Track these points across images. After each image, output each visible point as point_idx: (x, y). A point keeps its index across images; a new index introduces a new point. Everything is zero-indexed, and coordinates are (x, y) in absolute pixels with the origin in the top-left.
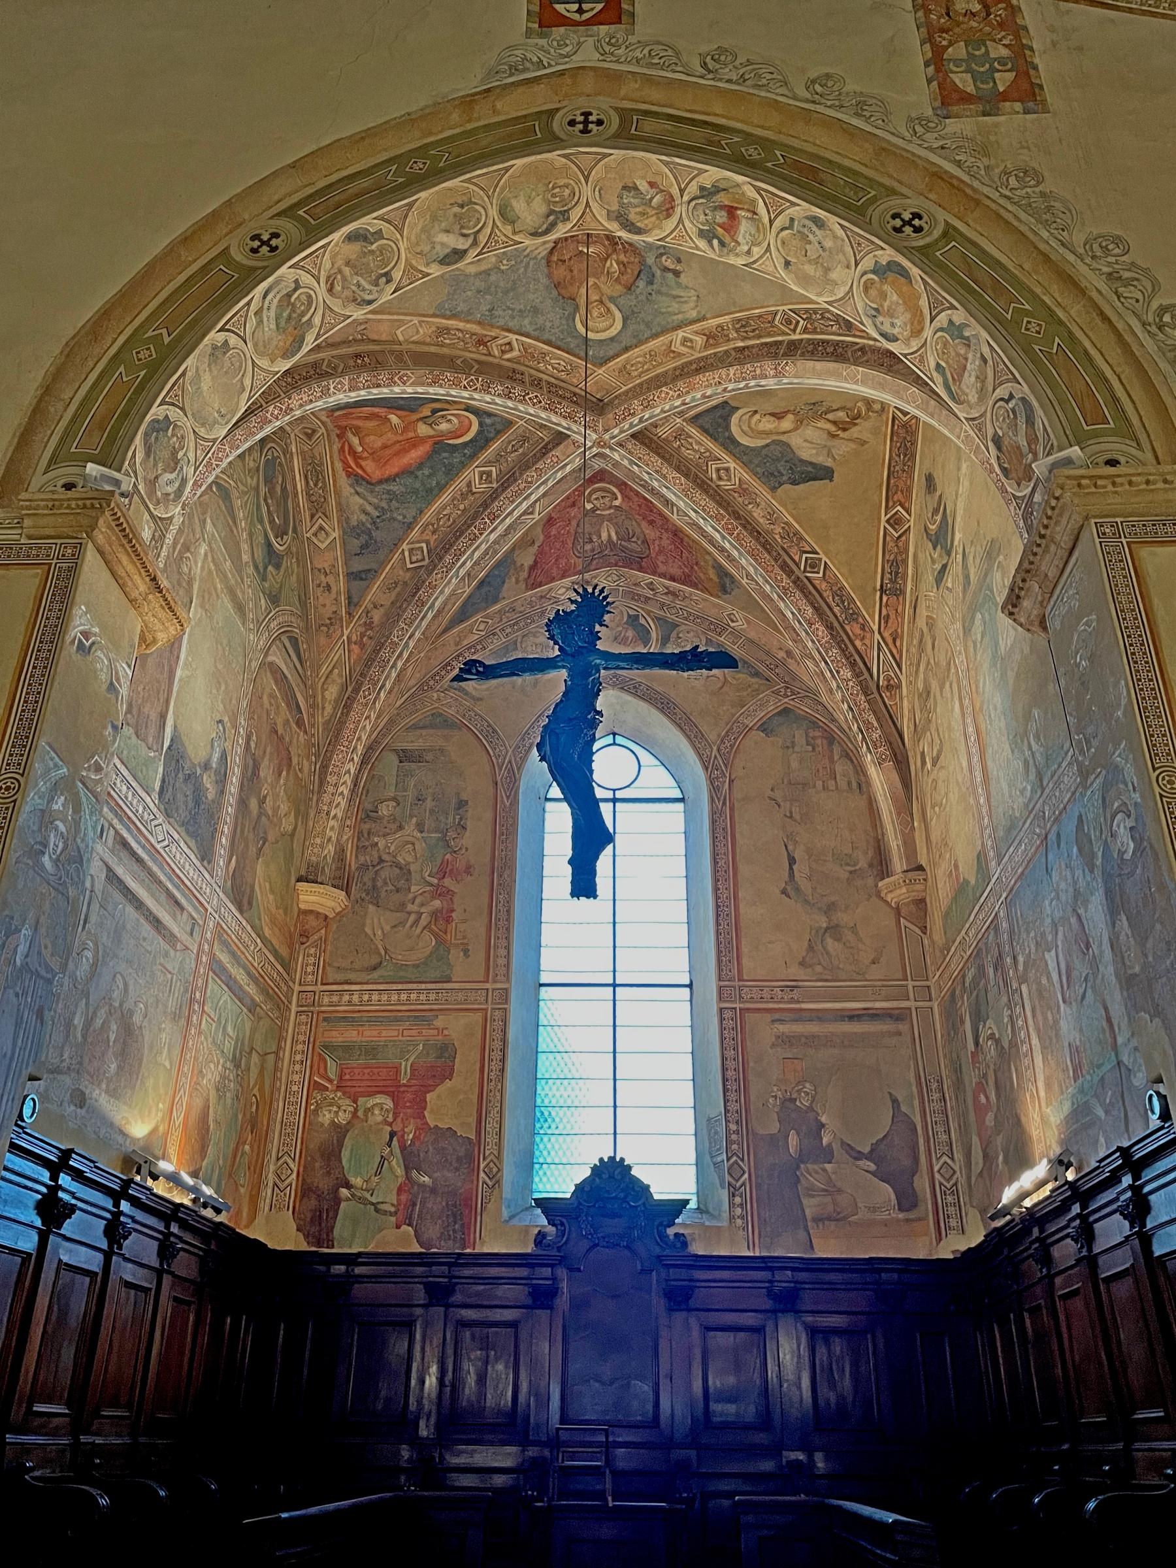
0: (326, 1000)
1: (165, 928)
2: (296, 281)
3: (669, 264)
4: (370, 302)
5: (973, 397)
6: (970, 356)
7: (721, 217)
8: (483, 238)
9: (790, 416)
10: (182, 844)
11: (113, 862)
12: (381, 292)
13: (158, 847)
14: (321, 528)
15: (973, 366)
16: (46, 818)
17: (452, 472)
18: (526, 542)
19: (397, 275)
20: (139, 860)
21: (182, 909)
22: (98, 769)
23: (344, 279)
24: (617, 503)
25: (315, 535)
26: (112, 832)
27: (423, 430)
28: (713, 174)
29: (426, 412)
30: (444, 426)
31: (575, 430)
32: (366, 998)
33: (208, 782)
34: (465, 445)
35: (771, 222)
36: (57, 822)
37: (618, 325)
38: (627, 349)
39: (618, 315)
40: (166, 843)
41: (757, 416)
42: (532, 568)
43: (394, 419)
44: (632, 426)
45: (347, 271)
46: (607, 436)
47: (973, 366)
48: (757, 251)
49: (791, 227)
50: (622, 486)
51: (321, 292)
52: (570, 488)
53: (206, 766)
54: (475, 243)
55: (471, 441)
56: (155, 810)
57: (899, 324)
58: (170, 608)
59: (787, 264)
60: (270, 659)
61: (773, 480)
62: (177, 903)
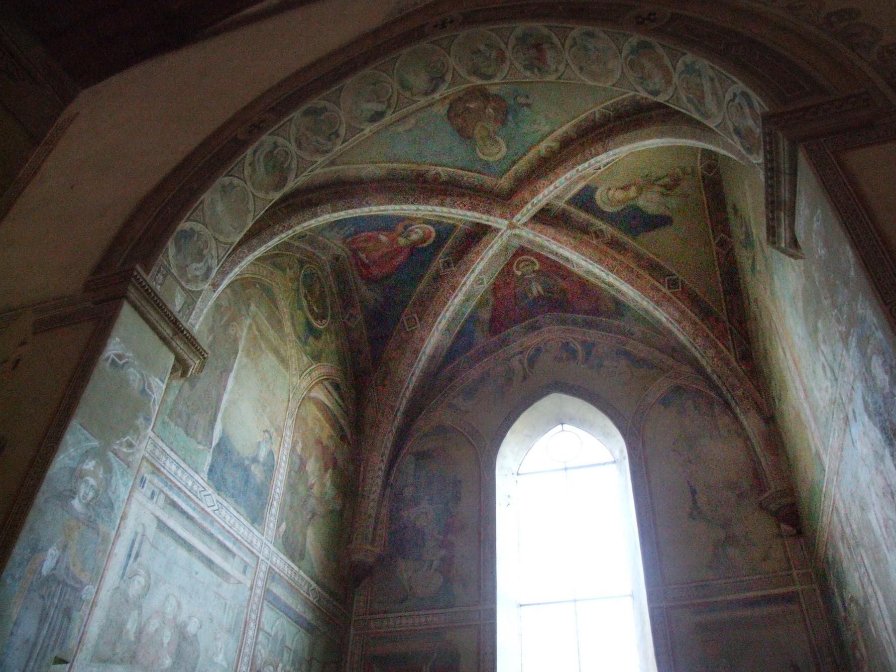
0: (372, 625)
1: (218, 567)
2: (275, 143)
3: (522, 100)
4: (327, 152)
5: (714, 110)
6: (704, 82)
7: (533, 53)
8: (393, 102)
9: (633, 188)
10: (232, 509)
11: (164, 517)
12: (334, 144)
13: (209, 510)
14: (351, 315)
15: (707, 87)
16: (77, 475)
17: (425, 265)
18: (482, 304)
19: (342, 132)
20: (190, 518)
21: (234, 555)
22: (130, 445)
23: (308, 138)
24: (537, 268)
25: (348, 320)
26: (162, 496)
27: (402, 241)
28: (520, 27)
29: (400, 228)
30: (414, 237)
31: (499, 223)
32: (398, 622)
33: (257, 471)
34: (429, 246)
35: (563, 45)
36: (88, 478)
37: (504, 149)
38: (514, 163)
39: (501, 142)
40: (216, 508)
41: (611, 192)
42: (492, 320)
43: (383, 238)
44: (528, 211)
45: (308, 134)
46: (514, 221)
47: (707, 87)
48: (561, 67)
49: (575, 43)
50: (539, 256)
51: (293, 147)
52: (502, 262)
53: (255, 460)
54: (389, 106)
55: (434, 241)
56: (205, 485)
57: (657, 81)
58: (192, 343)
59: (581, 69)
60: (313, 394)
61: (633, 231)
62: (228, 549)
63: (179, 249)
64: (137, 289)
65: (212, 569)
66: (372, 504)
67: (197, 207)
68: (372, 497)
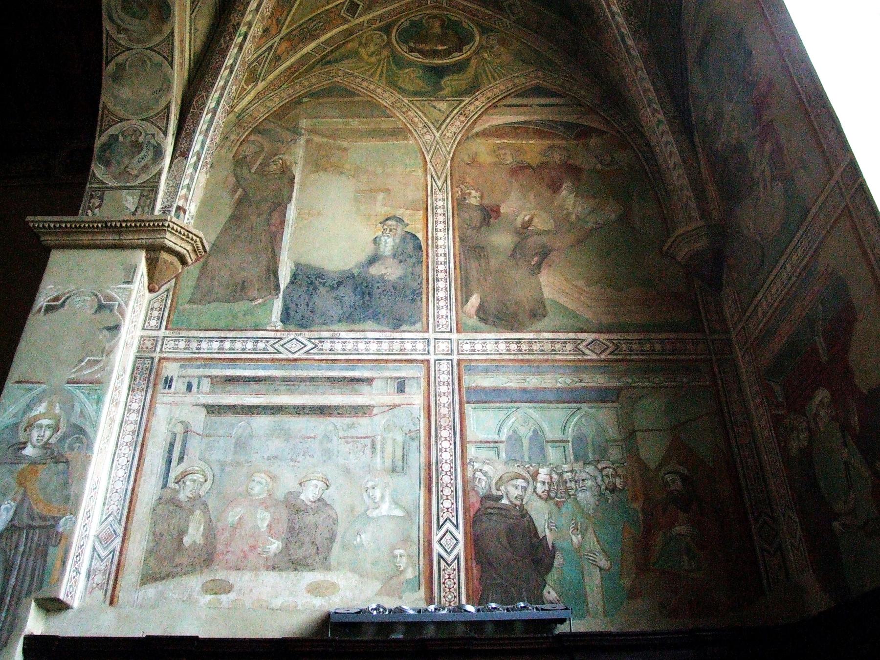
20: (257, 380)
21: (369, 381)
63: (107, 164)
64: (50, 233)
65: (330, 415)
66: (675, 174)
67: (102, 115)
68: (671, 164)
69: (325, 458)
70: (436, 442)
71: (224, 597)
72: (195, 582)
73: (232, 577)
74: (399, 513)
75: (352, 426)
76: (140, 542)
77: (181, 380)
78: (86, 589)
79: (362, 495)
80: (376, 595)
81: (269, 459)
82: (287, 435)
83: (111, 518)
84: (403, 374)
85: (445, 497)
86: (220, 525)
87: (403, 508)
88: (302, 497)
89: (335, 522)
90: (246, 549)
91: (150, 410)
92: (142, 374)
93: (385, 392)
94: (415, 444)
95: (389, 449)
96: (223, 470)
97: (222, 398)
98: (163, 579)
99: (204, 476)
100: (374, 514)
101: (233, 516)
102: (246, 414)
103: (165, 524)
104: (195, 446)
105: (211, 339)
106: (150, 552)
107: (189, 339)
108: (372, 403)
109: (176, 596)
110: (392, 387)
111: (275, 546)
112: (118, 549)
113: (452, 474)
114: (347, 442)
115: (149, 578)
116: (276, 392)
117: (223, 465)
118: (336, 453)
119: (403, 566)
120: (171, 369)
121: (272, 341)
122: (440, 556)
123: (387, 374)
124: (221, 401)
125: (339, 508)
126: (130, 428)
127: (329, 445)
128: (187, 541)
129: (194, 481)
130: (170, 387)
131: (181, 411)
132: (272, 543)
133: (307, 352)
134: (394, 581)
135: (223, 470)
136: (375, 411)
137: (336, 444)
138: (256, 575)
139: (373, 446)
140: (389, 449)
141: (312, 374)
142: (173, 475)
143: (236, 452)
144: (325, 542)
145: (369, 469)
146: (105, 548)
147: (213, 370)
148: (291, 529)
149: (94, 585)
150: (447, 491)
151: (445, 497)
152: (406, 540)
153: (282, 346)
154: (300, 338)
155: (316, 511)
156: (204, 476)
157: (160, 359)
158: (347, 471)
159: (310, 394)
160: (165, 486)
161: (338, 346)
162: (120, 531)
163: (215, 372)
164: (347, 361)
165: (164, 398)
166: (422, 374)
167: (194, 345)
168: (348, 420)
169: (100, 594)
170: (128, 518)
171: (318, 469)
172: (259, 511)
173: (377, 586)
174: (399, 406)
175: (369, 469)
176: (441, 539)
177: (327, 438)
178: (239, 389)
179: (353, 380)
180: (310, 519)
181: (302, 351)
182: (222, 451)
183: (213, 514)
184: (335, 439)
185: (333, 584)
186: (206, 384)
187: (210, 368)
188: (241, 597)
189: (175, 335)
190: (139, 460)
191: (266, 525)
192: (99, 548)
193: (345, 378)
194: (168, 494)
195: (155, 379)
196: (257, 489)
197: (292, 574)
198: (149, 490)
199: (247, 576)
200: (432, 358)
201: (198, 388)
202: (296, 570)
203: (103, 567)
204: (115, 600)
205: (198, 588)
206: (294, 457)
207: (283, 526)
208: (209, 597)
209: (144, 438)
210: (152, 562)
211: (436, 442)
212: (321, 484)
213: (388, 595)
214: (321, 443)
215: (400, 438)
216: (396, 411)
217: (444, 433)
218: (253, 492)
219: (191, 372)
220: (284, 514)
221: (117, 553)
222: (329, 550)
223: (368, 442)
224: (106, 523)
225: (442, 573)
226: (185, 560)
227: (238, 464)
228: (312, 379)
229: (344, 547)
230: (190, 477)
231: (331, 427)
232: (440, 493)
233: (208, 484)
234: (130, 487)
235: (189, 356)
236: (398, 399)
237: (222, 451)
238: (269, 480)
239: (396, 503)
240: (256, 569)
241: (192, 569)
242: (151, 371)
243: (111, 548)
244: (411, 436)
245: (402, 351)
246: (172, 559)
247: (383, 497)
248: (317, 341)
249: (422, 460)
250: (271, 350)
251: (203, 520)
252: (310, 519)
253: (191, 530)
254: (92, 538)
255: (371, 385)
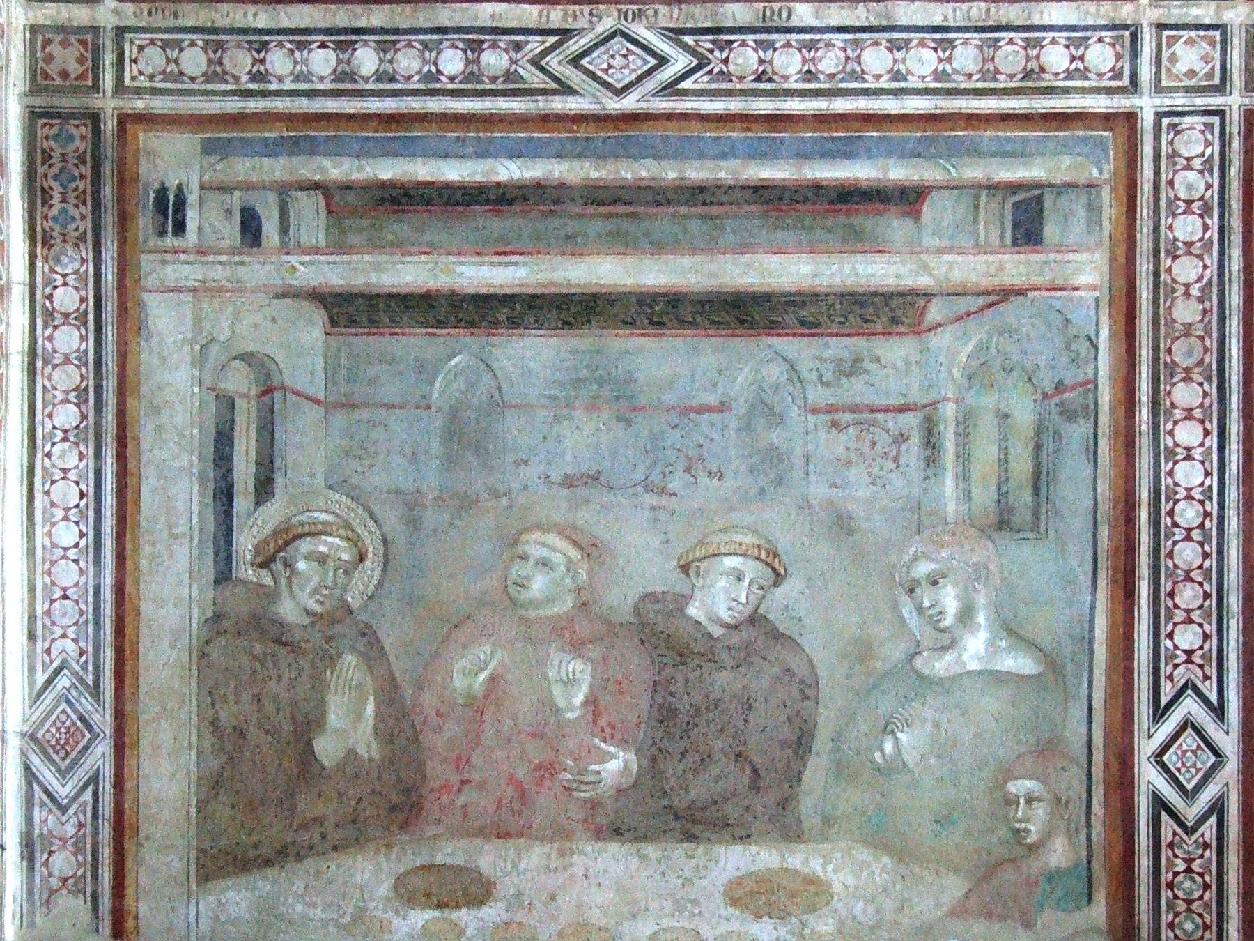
21: (909, 199)
65: (773, 327)
69: (762, 482)
70: (1155, 427)
71: (464, 916)
72: (370, 874)
73: (488, 858)
74: (1020, 663)
75: (853, 368)
76: (174, 754)
77: (214, 199)
78: (30, 892)
79: (896, 608)
80: (952, 913)
81: (568, 482)
82: (624, 401)
83: (63, 682)
84: (1036, 172)
85: (1179, 616)
86: (429, 700)
87: (1033, 646)
88: (693, 611)
89: (808, 688)
90: (521, 774)
91: (123, 308)
92: (64, 177)
93: (968, 243)
94: (1078, 431)
95: (986, 452)
96: (413, 523)
97: (377, 268)
98: (268, 863)
99: (355, 541)
100: (942, 666)
101: (468, 670)
102: (471, 324)
103: (246, 697)
104: (307, 445)
105: (300, 37)
106: (213, 786)
107: (215, 40)
108: (924, 281)
109: (318, 913)
110: (993, 223)
111: (616, 765)
112: (108, 770)
113: (1207, 538)
114: (835, 424)
115: (219, 862)
116: (572, 246)
117: (412, 505)
118: (798, 462)
119: (1034, 832)
120: (170, 160)
121: (535, 45)
122: (1159, 804)
123: (974, 172)
124: (373, 278)
125: (820, 648)
126: (66, 378)
127: (775, 437)
128: (327, 749)
129: (322, 560)
130: (180, 228)
131: (236, 317)
132: (605, 758)
133: (671, 89)
134: (1008, 876)
135: (413, 523)
136: (935, 312)
137: (800, 434)
138: (562, 853)
139: (931, 441)
140: (986, 452)
141: (697, 172)
142: (245, 543)
143: (451, 462)
144: (781, 755)
145: (920, 519)
146: (63, 774)
147: (326, 162)
148: (665, 715)
149: (54, 882)
150: (1188, 596)
151: (1179, 616)
152: (1047, 750)
153: (575, 61)
154: (641, 31)
155: (744, 658)
156: (355, 541)
157: (124, 120)
158: (842, 524)
159: (694, 251)
160: (224, 576)
161: (789, 63)
162: (103, 719)
163: (336, 169)
164: (822, 120)
165: (167, 271)
166: (1108, 168)
167: (240, 62)
168: (837, 347)
169: (78, 907)
170: (119, 675)
171: (736, 517)
172: (555, 656)
173: (955, 888)
174: (1020, 292)
175: (920, 519)
176: (1166, 747)
177: (765, 410)
178: (434, 234)
179: (850, 196)
180: (723, 681)
181: (650, 85)
182: (401, 456)
183: (400, 666)
184: (794, 413)
185: (812, 881)
186: (310, 217)
187: (313, 153)
188: (519, 917)
189: (158, 21)
190: (121, 492)
191: (579, 699)
192: (47, 775)
193: (817, 187)
194: (238, 604)
195: (121, 199)
196: (538, 585)
197: (679, 851)
198: (174, 593)
199: (536, 856)
200: (1146, 105)
201: (284, 230)
202: (689, 837)
203: (70, 830)
204: (130, 923)
205: (384, 889)
206: (655, 477)
207: (636, 705)
208: (420, 918)
209: (121, 413)
210: (223, 811)
211: (1155, 427)
212: (751, 569)
213: (989, 916)
214: (747, 427)
215: (1024, 411)
216: (1011, 311)
217: (1185, 395)
218: (525, 595)
219: (243, 168)
220: (636, 664)
221: (107, 787)
222: (794, 778)
223: (911, 421)
224: (49, 698)
225: (1165, 854)
226: (328, 810)
227: (467, 503)
228: (698, 194)
229: (843, 771)
230: (305, 546)
231: (776, 372)
232: (1165, 602)
233: (372, 567)
234: (108, 580)
235: (233, 105)
236: (1015, 267)
237: (401, 456)
238: (574, 554)
239: (1011, 630)
240: (559, 834)
241: (352, 835)
242: (97, 165)
243: (82, 773)
244: (1067, 402)
245: (1032, 79)
246: (286, 804)
247: (966, 615)
248: (706, 42)
249: (1103, 487)
250: (535, 79)
251: (369, 685)
252: (723, 681)
253: (334, 718)
254: (14, 743)
255: (916, 214)
